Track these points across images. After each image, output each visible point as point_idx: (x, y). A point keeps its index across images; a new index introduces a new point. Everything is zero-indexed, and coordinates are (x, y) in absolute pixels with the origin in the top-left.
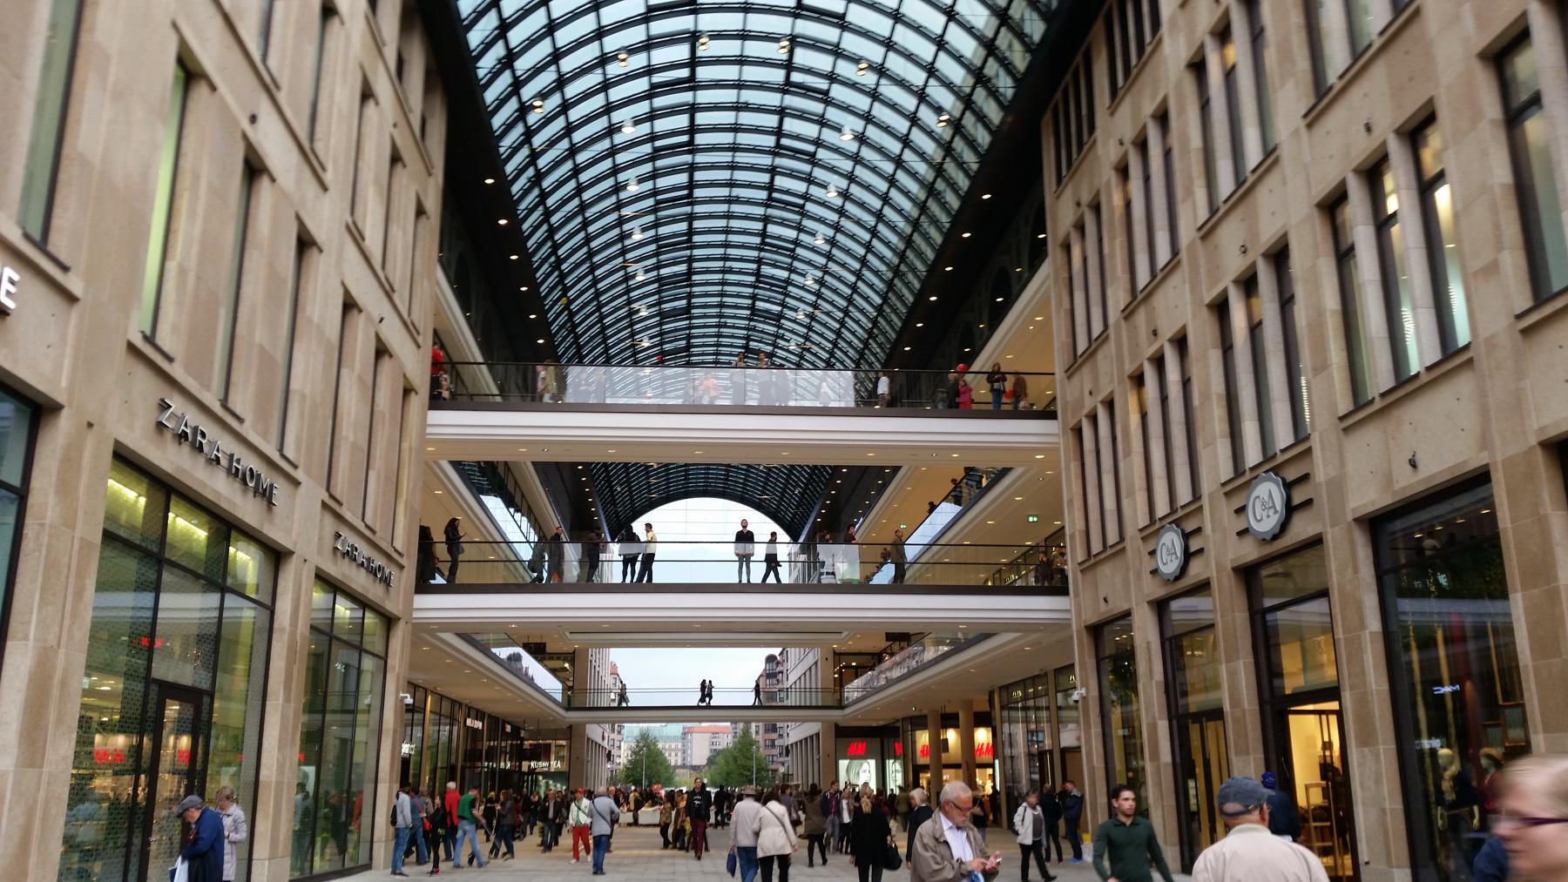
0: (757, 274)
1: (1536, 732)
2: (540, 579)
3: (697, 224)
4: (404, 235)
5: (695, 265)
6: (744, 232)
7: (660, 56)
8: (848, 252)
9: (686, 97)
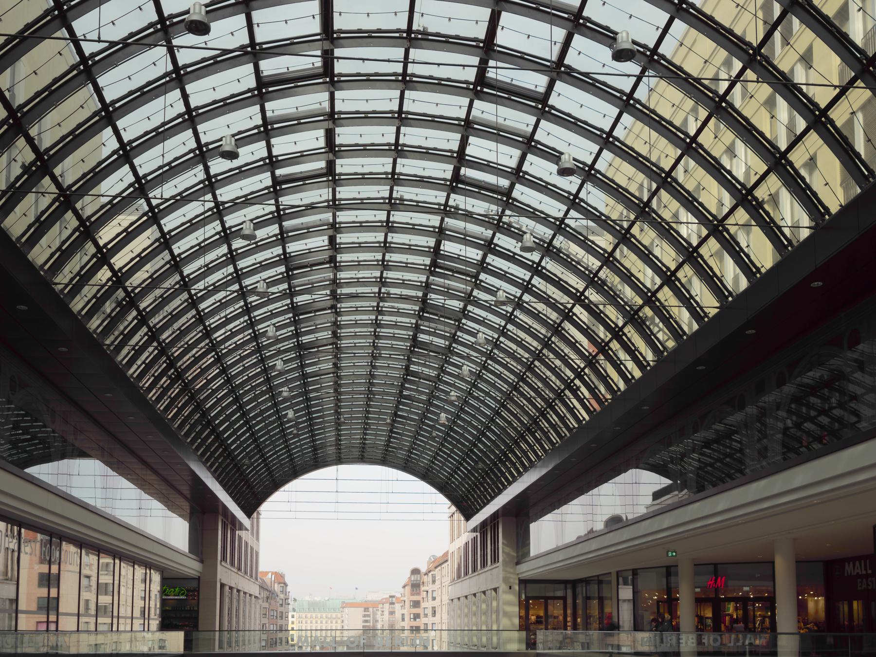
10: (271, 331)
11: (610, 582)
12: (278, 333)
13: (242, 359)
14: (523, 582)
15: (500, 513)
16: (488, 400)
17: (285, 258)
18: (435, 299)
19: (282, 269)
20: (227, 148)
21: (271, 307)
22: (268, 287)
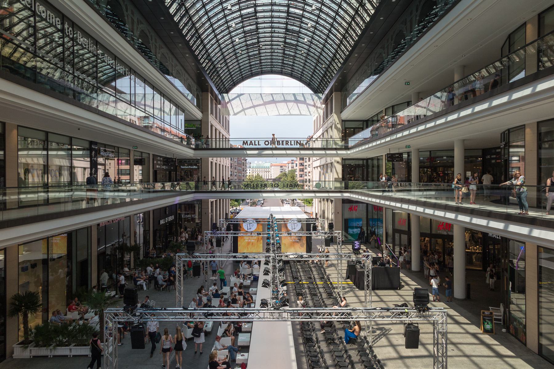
1: (64, 170)
4: (468, 338)
6: (280, 11)
8: (327, 14)
10: (237, 40)
14: (343, 122)
17: (244, 32)
18: (290, 27)
19: (240, 19)
21: (237, 31)
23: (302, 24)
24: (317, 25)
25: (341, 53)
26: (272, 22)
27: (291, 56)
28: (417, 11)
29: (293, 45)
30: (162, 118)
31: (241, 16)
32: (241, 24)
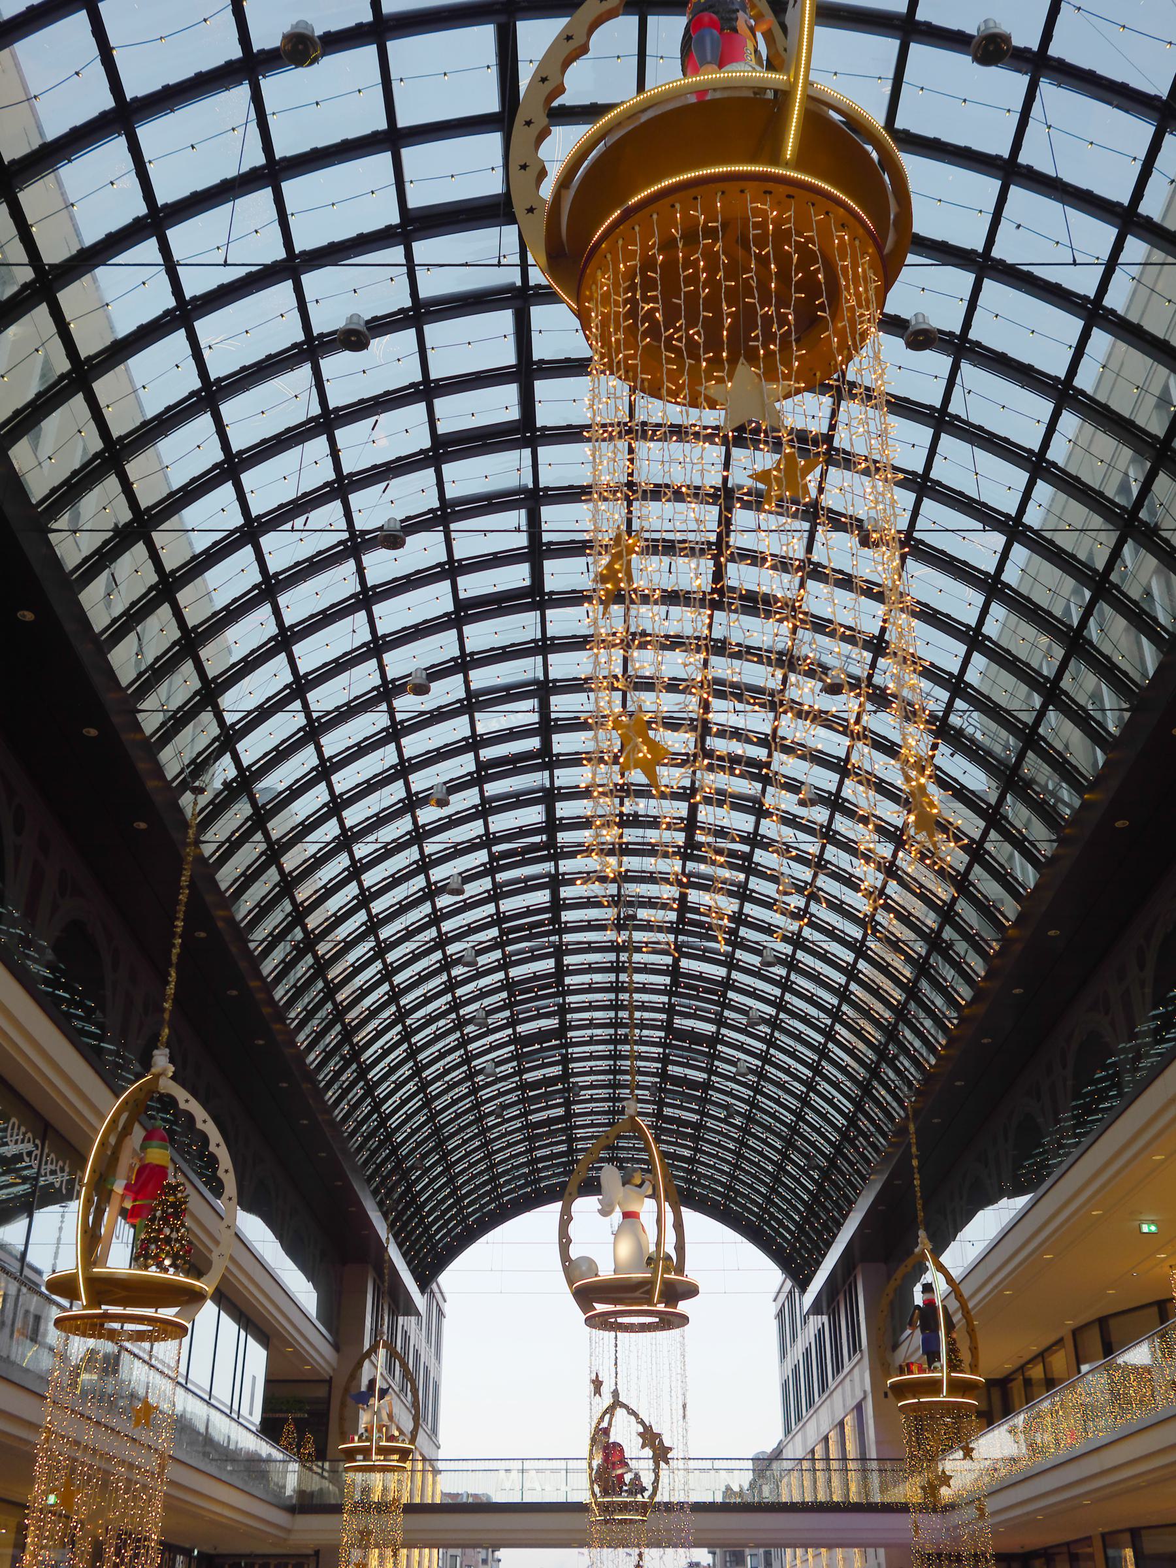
0: (668, 1027)
2: (151, 1100)
3: (566, 892)
5: (568, 960)
7: (471, 540)
9: (536, 779)
11: (1091, 1557)
12: (498, 1070)
13: (458, 1116)
15: (951, 1230)
16: (767, 1151)
20: (454, 886)
21: (491, 1038)
22: (496, 1067)
23: (726, 1013)
24: (782, 1016)
25: (876, 1113)
26: (614, 1071)
27: (687, 1124)
28: (1142, 967)
29: (693, 1084)
30: (235, 1407)
31: (508, 985)
32: (507, 1013)
